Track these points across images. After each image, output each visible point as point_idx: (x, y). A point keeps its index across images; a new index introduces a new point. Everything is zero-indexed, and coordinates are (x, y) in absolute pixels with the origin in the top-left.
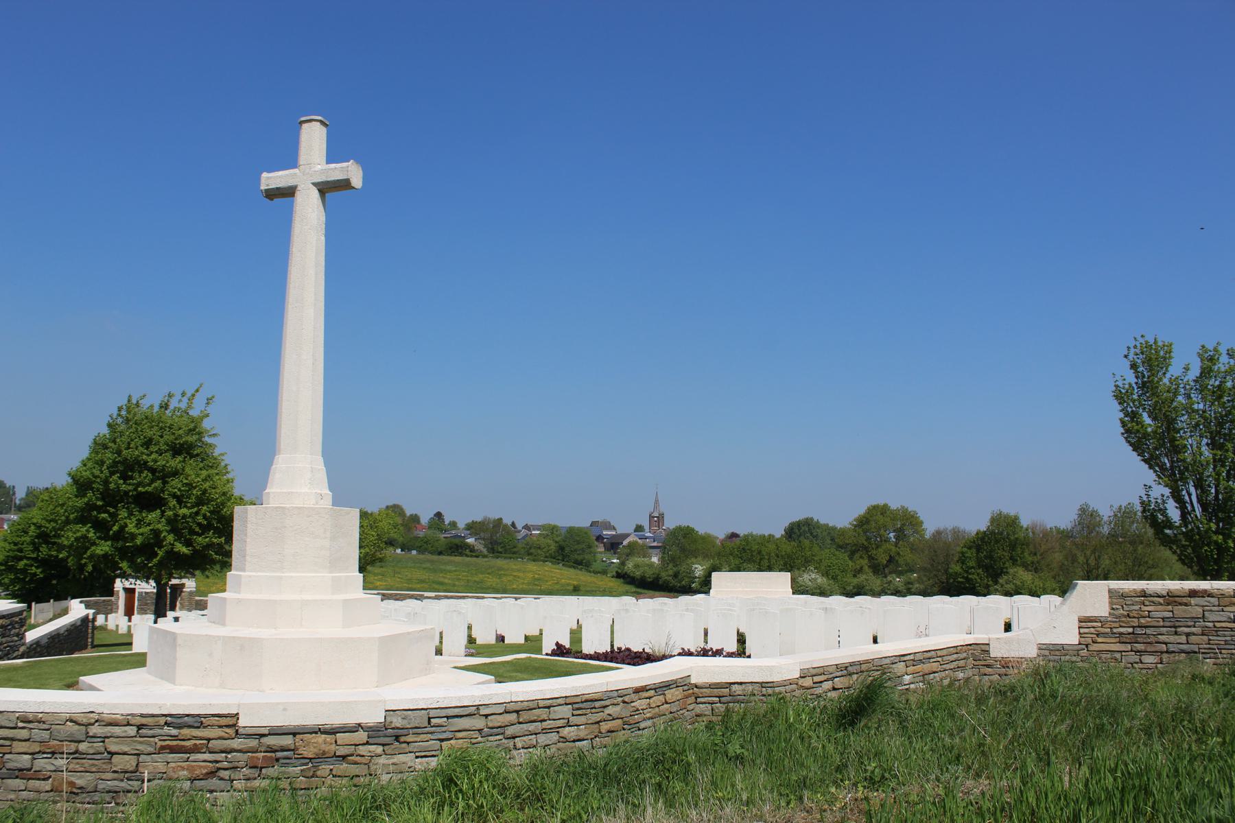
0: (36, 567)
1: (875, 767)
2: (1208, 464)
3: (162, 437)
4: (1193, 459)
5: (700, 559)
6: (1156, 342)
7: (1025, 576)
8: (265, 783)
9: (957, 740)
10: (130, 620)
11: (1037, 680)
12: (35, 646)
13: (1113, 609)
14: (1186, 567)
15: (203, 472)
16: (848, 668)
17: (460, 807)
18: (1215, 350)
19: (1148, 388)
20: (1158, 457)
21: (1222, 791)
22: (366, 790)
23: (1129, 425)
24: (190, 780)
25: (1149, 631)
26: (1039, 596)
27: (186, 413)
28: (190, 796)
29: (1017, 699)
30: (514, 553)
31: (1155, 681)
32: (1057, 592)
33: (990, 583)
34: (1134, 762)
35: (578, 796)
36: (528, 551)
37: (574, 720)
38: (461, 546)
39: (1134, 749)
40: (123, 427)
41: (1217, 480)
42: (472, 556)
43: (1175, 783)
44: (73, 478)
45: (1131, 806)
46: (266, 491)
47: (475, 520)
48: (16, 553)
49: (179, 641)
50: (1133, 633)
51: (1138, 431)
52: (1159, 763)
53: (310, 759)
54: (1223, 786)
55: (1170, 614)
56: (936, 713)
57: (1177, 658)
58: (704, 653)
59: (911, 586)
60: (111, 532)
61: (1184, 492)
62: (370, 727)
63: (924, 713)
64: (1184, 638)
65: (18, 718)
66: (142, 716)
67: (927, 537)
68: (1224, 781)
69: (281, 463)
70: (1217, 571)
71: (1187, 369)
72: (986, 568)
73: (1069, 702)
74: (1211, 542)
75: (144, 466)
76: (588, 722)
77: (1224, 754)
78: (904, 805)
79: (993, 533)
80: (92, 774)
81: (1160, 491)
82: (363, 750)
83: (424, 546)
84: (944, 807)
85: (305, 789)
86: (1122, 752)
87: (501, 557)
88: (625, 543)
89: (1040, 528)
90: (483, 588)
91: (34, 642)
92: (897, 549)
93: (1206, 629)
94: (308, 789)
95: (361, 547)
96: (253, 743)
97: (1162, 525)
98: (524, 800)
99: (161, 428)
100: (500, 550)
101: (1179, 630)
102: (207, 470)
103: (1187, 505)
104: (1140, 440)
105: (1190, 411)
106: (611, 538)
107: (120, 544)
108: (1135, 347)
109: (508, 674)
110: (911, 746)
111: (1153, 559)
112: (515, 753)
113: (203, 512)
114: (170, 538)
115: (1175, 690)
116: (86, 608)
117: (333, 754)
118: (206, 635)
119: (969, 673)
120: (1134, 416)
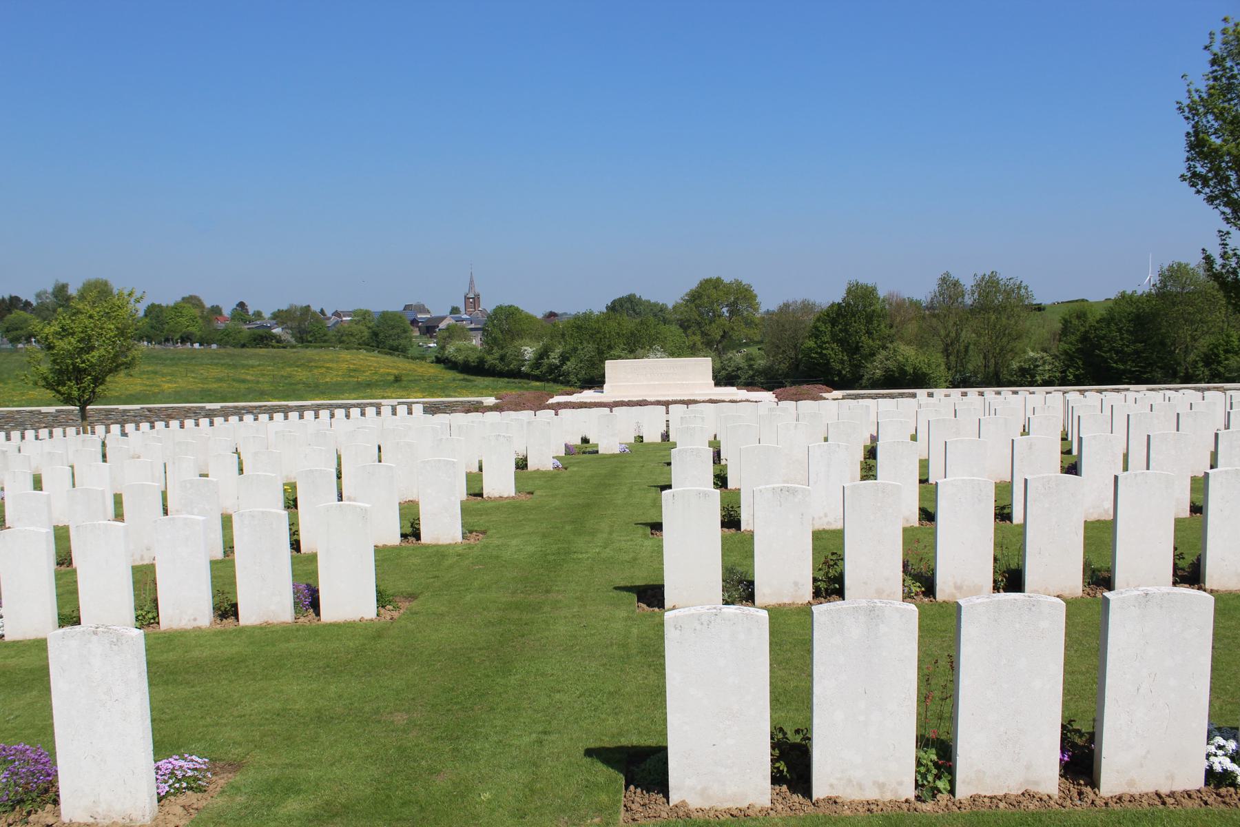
26: (183, 299)
30: (325, 341)
36: (339, 339)
38: (266, 337)
42: (278, 347)
47: (281, 309)
59: (752, 362)
72: (841, 342)
83: (226, 339)
87: (311, 347)
88: (442, 325)
100: (310, 339)
106: (427, 321)
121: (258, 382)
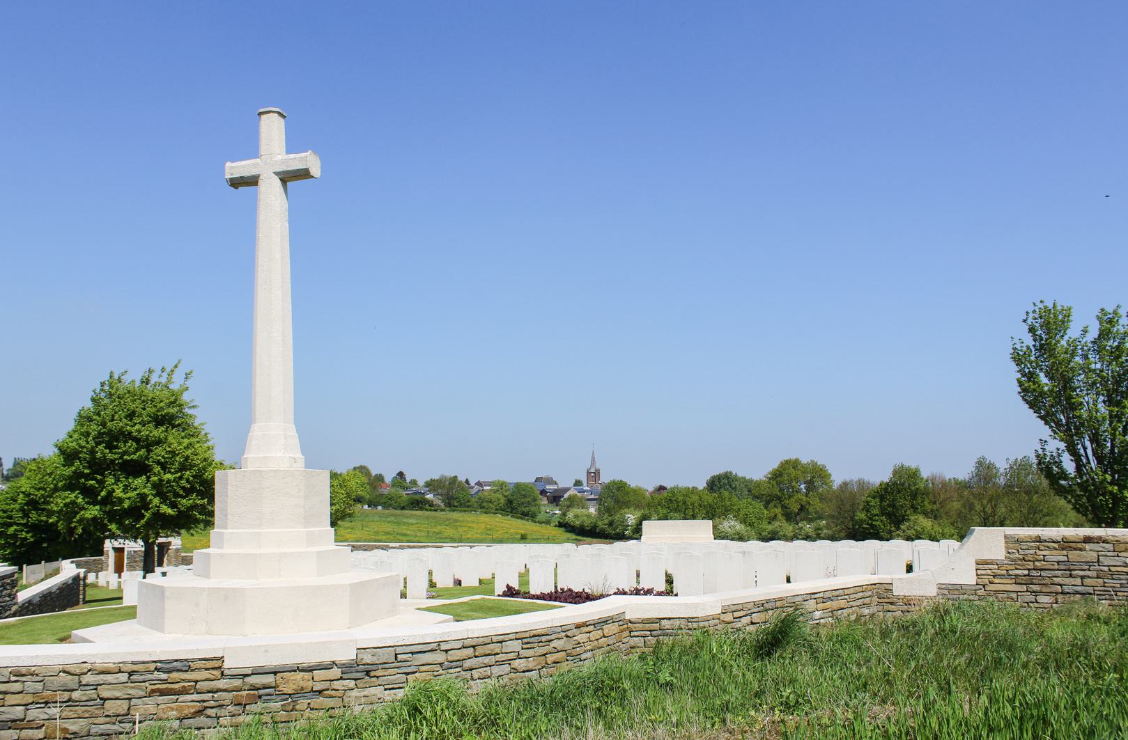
0: (26, 532)
1: (790, 693)
2: (1104, 419)
3: (144, 409)
4: (1088, 416)
5: (632, 509)
6: (1054, 306)
7: (925, 523)
8: (248, 719)
9: (864, 669)
10: (120, 577)
11: (937, 616)
12: (27, 604)
13: (1009, 553)
14: (1080, 515)
15: (184, 440)
16: (764, 605)
17: (424, 733)
18: (1115, 312)
19: (1045, 350)
20: (1054, 414)
21: (1121, 724)
22: (340, 720)
23: (1026, 385)
24: (179, 719)
25: (1043, 574)
26: (938, 541)
27: (166, 387)
28: (179, 734)
29: (918, 634)
30: (468, 507)
31: (1051, 620)
32: (955, 537)
33: (893, 529)
34: (1031, 693)
35: (528, 721)
37: (524, 653)
39: (1031, 681)
40: (106, 401)
41: (1114, 435)
42: (431, 510)
43: (1073, 715)
44: (59, 449)
45: (1030, 734)
46: (245, 456)
47: (433, 478)
48: (5, 519)
49: (167, 594)
50: (1029, 575)
51: (1035, 390)
52: (1056, 695)
53: (290, 694)
54: (1122, 719)
55: (1066, 559)
56: (844, 645)
57: (1072, 598)
58: (637, 592)
59: (820, 532)
60: (99, 497)
61: (1079, 446)
62: (344, 664)
63: (833, 645)
64: (1078, 581)
65: (11, 673)
66: (133, 663)
67: (835, 488)
68: (1123, 714)
69: (257, 431)
70: (1112, 519)
71: (1085, 331)
72: (889, 515)
73: (968, 637)
74: (1106, 492)
75: (128, 436)
76: (536, 655)
77: (1121, 689)
78: (817, 727)
79: (895, 484)
80: (85, 720)
81: (1055, 445)
82: (337, 685)
83: (389, 503)
84: (854, 730)
85: (285, 722)
86: (1019, 684)
87: (457, 510)
88: (566, 496)
89: (939, 479)
90: (441, 538)
91: (26, 601)
92: (808, 499)
93: (1102, 572)
94: (289, 722)
95: (331, 505)
96: (237, 683)
97: (1057, 476)
98: (480, 725)
99: (143, 401)
100: (456, 504)
101: (1073, 572)
102: (189, 439)
103: (1082, 458)
104: (1036, 398)
105: (1087, 370)
107: (108, 508)
108: (1034, 312)
109: (465, 614)
110: (822, 675)
111: (1048, 508)
112: (472, 683)
113: (186, 476)
114: (156, 501)
115: (1071, 628)
116: (77, 568)
117: (310, 689)
118: (193, 587)
119: (874, 609)
120: (1031, 376)
121: (416, 536)
